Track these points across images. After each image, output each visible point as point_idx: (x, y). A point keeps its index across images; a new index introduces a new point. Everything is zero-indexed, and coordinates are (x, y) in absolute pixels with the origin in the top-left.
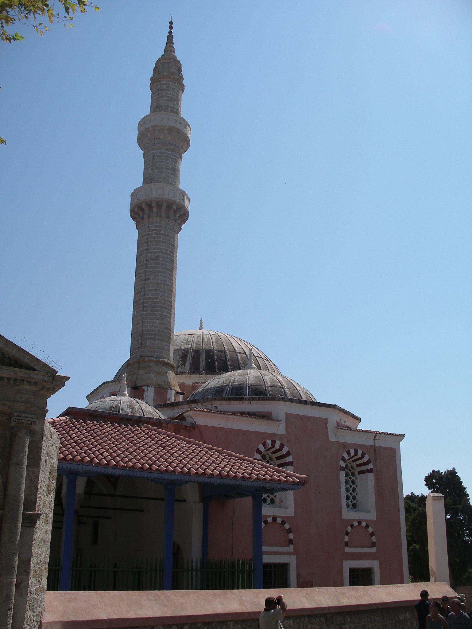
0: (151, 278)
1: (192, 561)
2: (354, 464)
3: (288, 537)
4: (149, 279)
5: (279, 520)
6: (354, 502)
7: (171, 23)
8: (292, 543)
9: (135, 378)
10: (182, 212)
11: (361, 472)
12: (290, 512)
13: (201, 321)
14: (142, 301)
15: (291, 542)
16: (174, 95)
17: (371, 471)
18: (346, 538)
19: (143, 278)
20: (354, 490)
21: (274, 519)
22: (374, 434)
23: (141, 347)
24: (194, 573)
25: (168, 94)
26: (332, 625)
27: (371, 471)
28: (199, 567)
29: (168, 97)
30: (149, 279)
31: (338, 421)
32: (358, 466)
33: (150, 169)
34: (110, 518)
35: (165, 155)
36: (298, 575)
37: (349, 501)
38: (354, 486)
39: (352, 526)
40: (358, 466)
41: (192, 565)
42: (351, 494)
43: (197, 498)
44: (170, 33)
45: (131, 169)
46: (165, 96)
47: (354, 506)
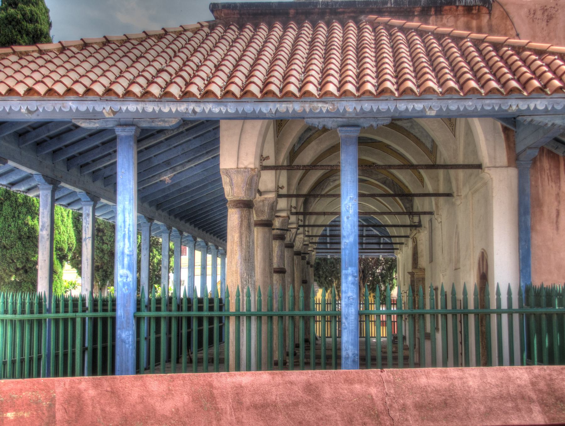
24: (505, 317)
28: (515, 306)
43: (502, 156)
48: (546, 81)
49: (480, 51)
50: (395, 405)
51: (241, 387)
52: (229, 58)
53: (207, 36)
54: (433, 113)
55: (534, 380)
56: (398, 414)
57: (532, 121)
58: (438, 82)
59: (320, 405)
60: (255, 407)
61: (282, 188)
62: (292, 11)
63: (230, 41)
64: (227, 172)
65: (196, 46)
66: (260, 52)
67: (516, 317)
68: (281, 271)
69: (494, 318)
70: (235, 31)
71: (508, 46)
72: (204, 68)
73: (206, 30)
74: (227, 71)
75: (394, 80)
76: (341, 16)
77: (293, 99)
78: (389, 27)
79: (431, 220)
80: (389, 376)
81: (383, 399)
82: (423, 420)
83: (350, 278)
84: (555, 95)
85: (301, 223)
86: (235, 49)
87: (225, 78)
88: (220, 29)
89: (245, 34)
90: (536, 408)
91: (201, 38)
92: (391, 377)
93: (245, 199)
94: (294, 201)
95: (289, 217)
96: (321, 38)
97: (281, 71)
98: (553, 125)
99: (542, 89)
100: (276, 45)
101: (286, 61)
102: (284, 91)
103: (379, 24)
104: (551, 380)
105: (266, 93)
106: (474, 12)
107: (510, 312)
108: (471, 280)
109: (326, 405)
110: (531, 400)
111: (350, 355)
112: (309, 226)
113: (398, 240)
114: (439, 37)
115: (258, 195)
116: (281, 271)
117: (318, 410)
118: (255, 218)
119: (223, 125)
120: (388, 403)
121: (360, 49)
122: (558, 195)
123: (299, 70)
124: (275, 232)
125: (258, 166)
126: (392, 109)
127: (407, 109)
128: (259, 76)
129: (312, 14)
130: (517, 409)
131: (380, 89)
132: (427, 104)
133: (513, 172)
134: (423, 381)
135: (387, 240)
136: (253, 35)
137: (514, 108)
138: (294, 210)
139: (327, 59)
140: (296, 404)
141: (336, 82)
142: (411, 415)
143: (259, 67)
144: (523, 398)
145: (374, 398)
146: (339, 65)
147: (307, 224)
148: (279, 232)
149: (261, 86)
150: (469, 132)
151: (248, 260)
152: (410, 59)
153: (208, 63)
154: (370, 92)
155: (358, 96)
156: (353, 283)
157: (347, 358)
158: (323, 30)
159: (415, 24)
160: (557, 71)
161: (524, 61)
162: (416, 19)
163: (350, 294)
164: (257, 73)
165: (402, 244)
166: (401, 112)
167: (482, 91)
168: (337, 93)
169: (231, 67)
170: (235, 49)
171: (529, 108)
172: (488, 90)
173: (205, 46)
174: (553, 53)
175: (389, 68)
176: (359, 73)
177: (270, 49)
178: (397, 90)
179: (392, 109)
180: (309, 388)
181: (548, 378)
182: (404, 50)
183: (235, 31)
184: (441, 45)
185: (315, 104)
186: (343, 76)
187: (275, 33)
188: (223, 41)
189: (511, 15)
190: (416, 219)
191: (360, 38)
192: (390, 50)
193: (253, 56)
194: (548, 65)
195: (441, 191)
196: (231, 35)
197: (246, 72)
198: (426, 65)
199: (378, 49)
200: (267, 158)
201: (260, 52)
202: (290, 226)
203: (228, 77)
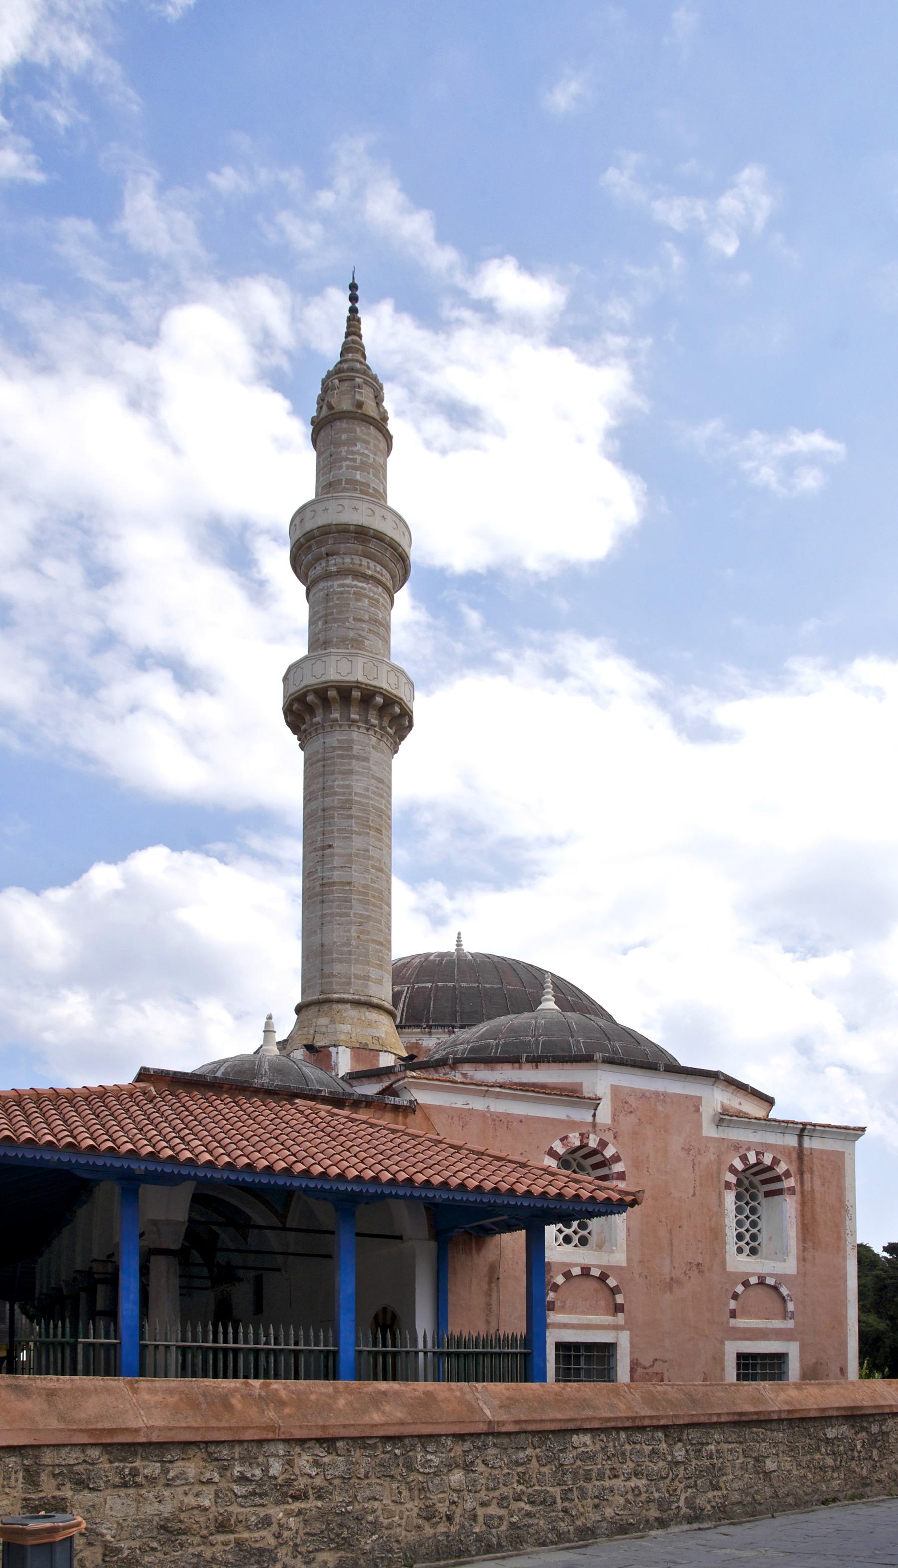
0: (335, 845)
2: (756, 1180)
4: (330, 846)
6: (753, 1244)
8: (622, 1311)
9: (312, 1032)
11: (768, 1194)
12: (619, 1258)
14: (318, 889)
15: (618, 1309)
16: (367, 456)
17: (792, 1190)
18: (733, 1305)
19: (319, 844)
20: (754, 1224)
23: (322, 976)
25: (353, 453)
26: (680, 1444)
27: (792, 1190)
29: (354, 460)
30: (330, 846)
32: (764, 1182)
33: (320, 623)
34: (279, 1270)
35: (352, 590)
36: (632, 1362)
37: (742, 1243)
39: (746, 1284)
40: (764, 1182)
42: (747, 1217)
46: (346, 459)
47: (754, 1251)
133: (432, 1245)
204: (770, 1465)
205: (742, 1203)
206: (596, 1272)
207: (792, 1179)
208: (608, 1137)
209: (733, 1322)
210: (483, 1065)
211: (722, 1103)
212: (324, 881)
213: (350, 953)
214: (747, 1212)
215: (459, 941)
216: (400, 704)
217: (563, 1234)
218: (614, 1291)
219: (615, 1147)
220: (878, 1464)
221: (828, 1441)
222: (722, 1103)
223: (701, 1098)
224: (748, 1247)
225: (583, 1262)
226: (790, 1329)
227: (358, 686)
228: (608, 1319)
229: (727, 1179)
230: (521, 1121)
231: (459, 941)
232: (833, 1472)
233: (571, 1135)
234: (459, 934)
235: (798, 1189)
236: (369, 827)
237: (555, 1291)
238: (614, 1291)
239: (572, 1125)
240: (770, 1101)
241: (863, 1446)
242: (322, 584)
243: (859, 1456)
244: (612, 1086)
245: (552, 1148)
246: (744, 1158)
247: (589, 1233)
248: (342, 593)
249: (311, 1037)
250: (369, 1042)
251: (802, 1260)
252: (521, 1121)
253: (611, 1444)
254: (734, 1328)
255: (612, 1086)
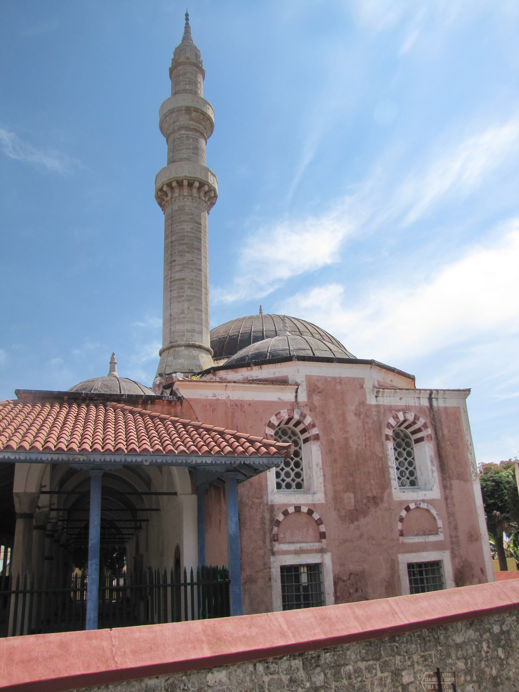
1: (165, 573)
2: (408, 431)
3: (319, 529)
4: (174, 261)
5: (304, 509)
6: (411, 478)
7: (187, 15)
10: (212, 194)
11: (417, 441)
12: (319, 498)
13: (261, 308)
15: (323, 536)
16: (192, 79)
21: (298, 509)
22: (429, 392)
24: (189, 587)
26: (318, 669)
28: (195, 580)
29: (186, 81)
30: (174, 261)
31: (380, 380)
32: (413, 433)
38: (409, 459)
39: (408, 509)
40: (413, 433)
41: (159, 579)
43: (188, 488)
44: (187, 24)
45: (154, 157)
48: (211, 447)
49: (175, 428)
50: (119, 653)
51: (14, 647)
52: (24, 424)
53: (12, 409)
54: (148, 464)
55: (205, 628)
56: (120, 659)
57: (204, 469)
58: (151, 445)
59: (68, 656)
60: (23, 662)
61: (54, 504)
62: (66, 397)
63: (26, 413)
64: (18, 494)
65: (4, 415)
66: (44, 421)
67: (195, 587)
68: (50, 558)
69: (182, 588)
70: (29, 407)
71: (191, 425)
72: (7, 430)
73: (12, 405)
74: (22, 432)
75: (125, 443)
76: (96, 402)
77: (62, 452)
78: (123, 410)
79: (147, 525)
80: (115, 633)
81: (111, 649)
82: (136, 661)
83: (94, 566)
84: (216, 455)
85: (65, 526)
86: (28, 419)
87: (21, 437)
88: (20, 406)
89: (35, 409)
90: (205, 646)
91: (7, 410)
92: (117, 634)
93: (28, 512)
94: (61, 513)
95: (57, 523)
96: (83, 415)
97: (57, 434)
98: (216, 471)
99: (209, 452)
100: (55, 417)
101: (60, 428)
102: (57, 447)
103: (118, 408)
104: (215, 627)
105: (46, 448)
106: (173, 404)
107: (192, 584)
108: (170, 565)
109: (72, 656)
110: (202, 642)
111: (92, 617)
112: (70, 528)
113: (127, 536)
114: (152, 418)
115: (37, 509)
116: (50, 558)
117: (66, 660)
118: (34, 523)
119: (17, 465)
120: (114, 651)
121: (105, 422)
122: (220, 510)
123: (68, 434)
124: (47, 533)
125: (38, 491)
126: (123, 460)
127: (132, 461)
128: (42, 437)
129: (79, 399)
130: (194, 648)
131: (116, 448)
132: (144, 458)
133: (195, 497)
134: (137, 635)
135: (121, 536)
136: (41, 410)
137: (194, 462)
138: (61, 518)
139: (85, 427)
140: (51, 657)
141: (90, 443)
142: (129, 659)
143: (42, 431)
144: (198, 640)
145: (105, 648)
146: (92, 432)
147: (69, 526)
148: (50, 532)
149: (43, 443)
150: (170, 474)
151: (28, 553)
152: (135, 430)
153: (10, 427)
154: (110, 450)
155: (103, 452)
156: (96, 569)
157: (90, 619)
158: (84, 409)
159: (138, 409)
160: (217, 441)
161: (200, 434)
162: (140, 406)
163: (93, 576)
164: (40, 435)
165: (129, 538)
166: (128, 462)
167: (176, 451)
168: (90, 450)
169: (25, 430)
170: (28, 419)
171: (202, 462)
172: (180, 451)
173: (9, 415)
174: (215, 431)
175: (123, 436)
176: (104, 438)
177: (51, 419)
178: (126, 449)
179: (123, 460)
180: (62, 645)
181: (213, 626)
182: (132, 424)
183: (29, 407)
184: (153, 422)
185: (76, 456)
186: (94, 439)
187: (54, 410)
188: (21, 413)
189: (193, 407)
190: (138, 524)
191: (106, 415)
192: (124, 424)
193: (39, 424)
194: (213, 438)
195: (154, 507)
196: (27, 410)
197: (34, 434)
198: (144, 434)
199: (116, 423)
200: (45, 486)
201: (44, 421)
202: (58, 528)
203: (22, 436)
204: (406, 678)
205: (401, 449)
206: (304, 509)
207: (308, 417)
208: (306, 411)
209: (401, 538)
210: (230, 370)
211: (378, 381)
212: (172, 279)
213: (184, 318)
214: (405, 455)
215: (261, 310)
216: (208, 185)
217: (285, 482)
218: (319, 522)
219: (311, 417)
220: (505, 662)
221: (458, 646)
222: (378, 381)
223: (363, 379)
224: (408, 481)
225: (295, 503)
226: (441, 541)
227: (186, 178)
228: (316, 545)
229: (386, 433)
230: (250, 405)
231: (261, 310)
232: (466, 675)
233: (282, 411)
234: (261, 306)
235: (433, 436)
236: (194, 248)
237: (278, 526)
238: (319, 522)
239: (281, 404)
240: (412, 378)
241: (488, 647)
242: (172, 135)
243: (487, 657)
244: (306, 376)
245: (270, 421)
246: (396, 418)
247: (415, 478)
248: (180, 138)
249: (164, 369)
250: (194, 368)
251: (445, 487)
252: (250, 405)
253: (248, 678)
254: (403, 543)
255: (306, 376)
